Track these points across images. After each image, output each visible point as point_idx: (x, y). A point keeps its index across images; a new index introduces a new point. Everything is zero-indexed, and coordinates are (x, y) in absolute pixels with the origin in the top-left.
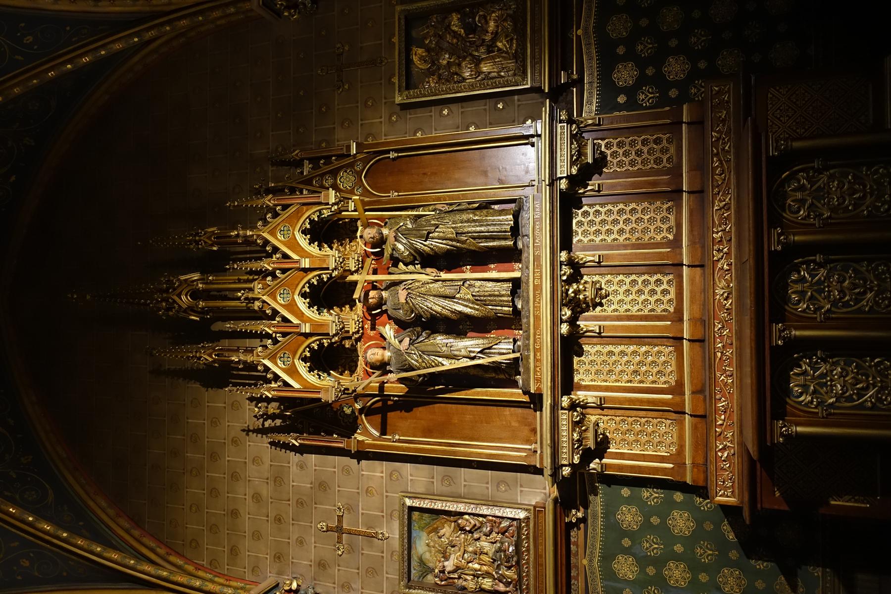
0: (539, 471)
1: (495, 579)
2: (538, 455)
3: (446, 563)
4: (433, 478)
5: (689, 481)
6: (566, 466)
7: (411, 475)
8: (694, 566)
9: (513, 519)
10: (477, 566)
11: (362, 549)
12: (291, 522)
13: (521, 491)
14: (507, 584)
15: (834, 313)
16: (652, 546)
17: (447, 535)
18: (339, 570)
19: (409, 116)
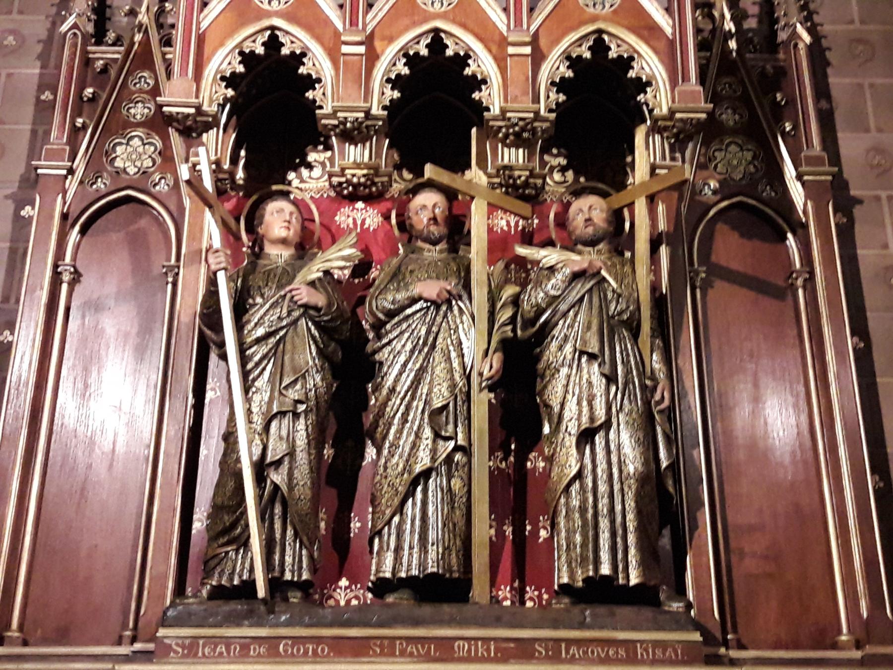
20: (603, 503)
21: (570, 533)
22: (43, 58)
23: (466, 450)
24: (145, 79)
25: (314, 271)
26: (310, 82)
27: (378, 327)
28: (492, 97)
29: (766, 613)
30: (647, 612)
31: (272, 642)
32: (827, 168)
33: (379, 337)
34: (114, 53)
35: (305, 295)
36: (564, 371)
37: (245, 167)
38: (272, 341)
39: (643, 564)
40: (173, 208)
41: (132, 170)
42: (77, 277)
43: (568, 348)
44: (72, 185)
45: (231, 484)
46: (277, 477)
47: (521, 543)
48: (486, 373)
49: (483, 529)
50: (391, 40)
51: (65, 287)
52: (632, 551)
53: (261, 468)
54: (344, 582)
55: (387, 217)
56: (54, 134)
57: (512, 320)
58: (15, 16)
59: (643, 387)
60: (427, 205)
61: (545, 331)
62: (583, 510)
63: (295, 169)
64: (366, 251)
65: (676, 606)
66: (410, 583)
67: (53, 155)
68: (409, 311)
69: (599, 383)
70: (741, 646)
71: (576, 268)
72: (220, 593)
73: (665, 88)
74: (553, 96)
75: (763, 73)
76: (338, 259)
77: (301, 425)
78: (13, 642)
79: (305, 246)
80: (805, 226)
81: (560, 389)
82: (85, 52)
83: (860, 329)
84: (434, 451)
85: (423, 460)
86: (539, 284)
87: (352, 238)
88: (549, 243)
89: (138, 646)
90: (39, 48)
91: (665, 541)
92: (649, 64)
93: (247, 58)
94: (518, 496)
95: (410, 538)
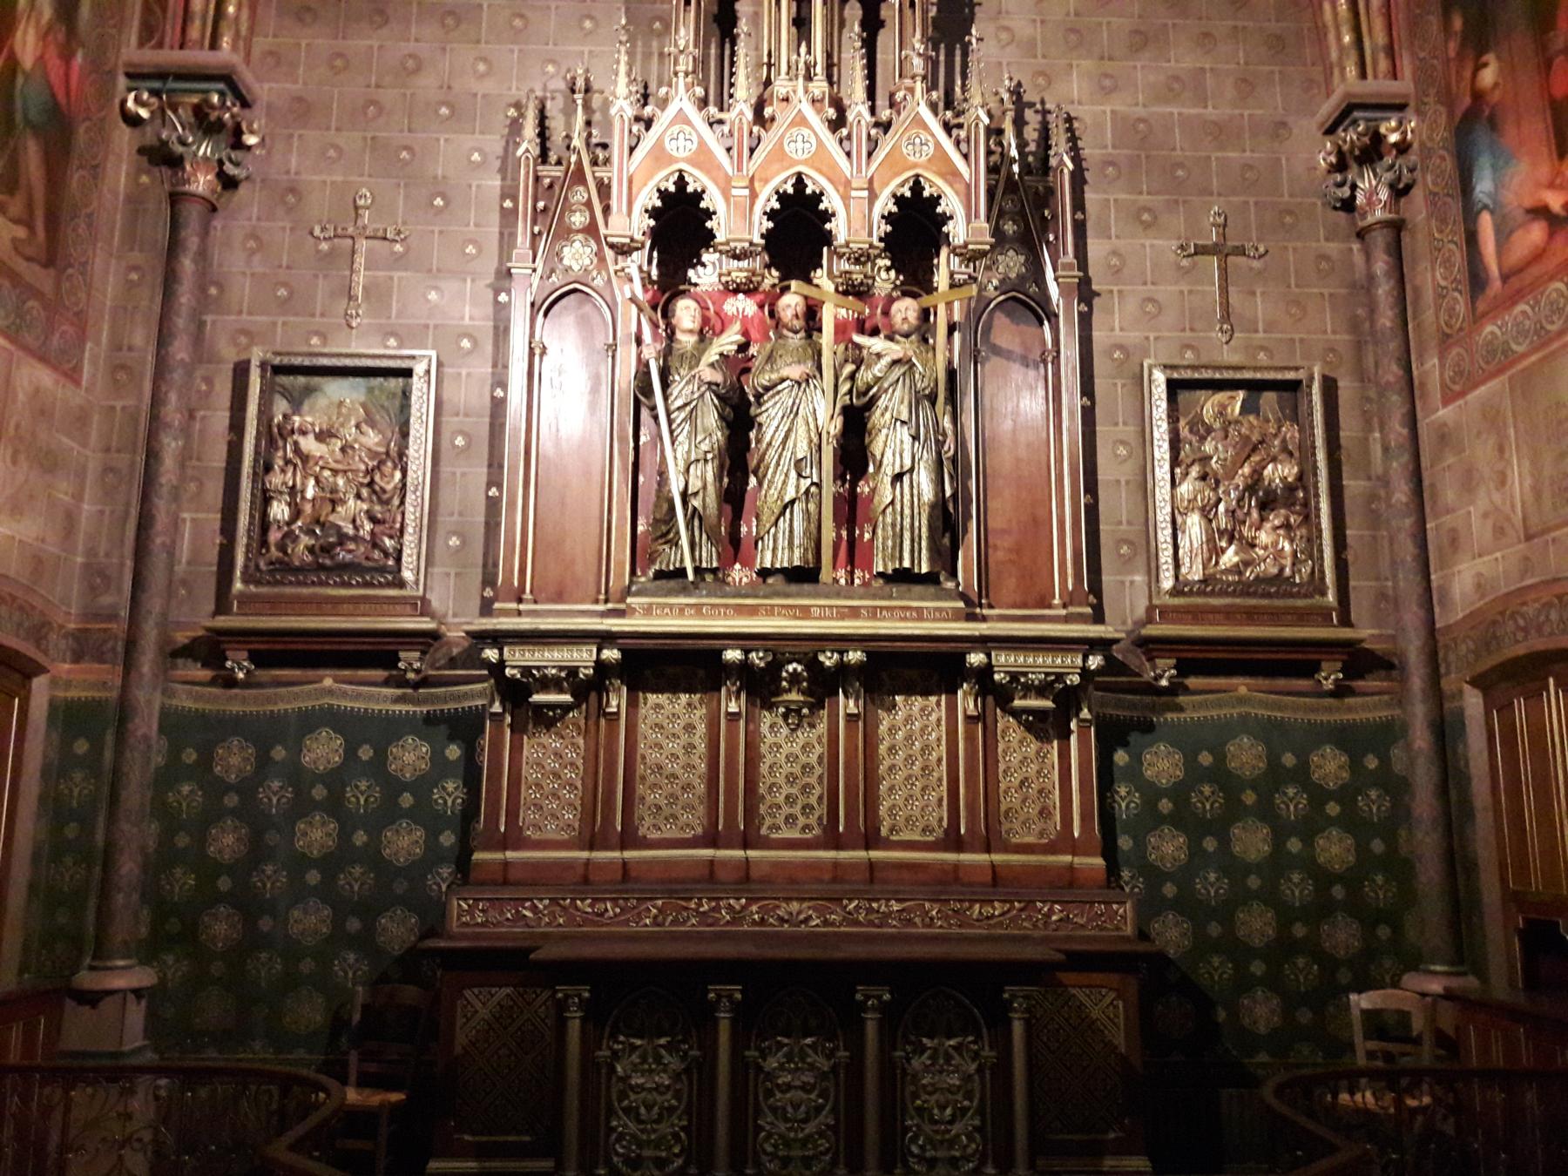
0: (486, 609)
1: (289, 524)
2: (513, 605)
3: (311, 437)
4: (466, 415)
5: (478, 856)
6: (501, 654)
7: (469, 375)
8: (332, 863)
9: (398, 560)
10: (310, 494)
11: (325, 276)
12: (369, 135)
13: (448, 575)
14: (282, 547)
15: (757, 1076)
16: (361, 794)
17: (363, 439)
18: (284, 229)
19: (1119, 383)
20: (907, 522)
21: (885, 539)
22: (503, 171)
23: (818, 485)
24: (579, 194)
25: (712, 355)
26: (709, 214)
27: (758, 396)
28: (839, 228)
29: (1008, 585)
30: (932, 589)
31: (698, 607)
32: (1076, 273)
33: (760, 405)
34: (557, 172)
35: (710, 375)
36: (884, 431)
37: (658, 266)
38: (688, 409)
39: (931, 560)
40: (608, 299)
41: (576, 268)
42: (544, 351)
43: (888, 415)
44: (536, 280)
45: (665, 506)
46: (696, 502)
47: (852, 542)
48: (832, 432)
49: (828, 534)
50: (766, 181)
51: (537, 358)
52: (924, 551)
53: (685, 496)
54: (737, 566)
55: (761, 307)
56: (519, 239)
57: (850, 392)
58: (477, 136)
59: (937, 441)
60: (791, 304)
61: (873, 401)
62: (893, 525)
63: (694, 266)
64: (745, 333)
65: (950, 585)
66: (783, 571)
67: (521, 258)
68: (780, 388)
69: (908, 440)
70: (991, 606)
71: (895, 357)
72: (660, 575)
73: (964, 224)
74: (883, 227)
75: (1037, 193)
76: (728, 341)
77: (709, 467)
78: (528, 601)
79: (705, 333)
80: (1057, 316)
81: (881, 444)
82: (535, 171)
83: (1088, 389)
84: (798, 487)
85: (790, 494)
86: (869, 367)
87: (737, 327)
88: (875, 332)
89: (610, 606)
90: (498, 164)
91: (946, 541)
92: (951, 203)
93: (663, 194)
94: (851, 510)
95: (782, 542)
